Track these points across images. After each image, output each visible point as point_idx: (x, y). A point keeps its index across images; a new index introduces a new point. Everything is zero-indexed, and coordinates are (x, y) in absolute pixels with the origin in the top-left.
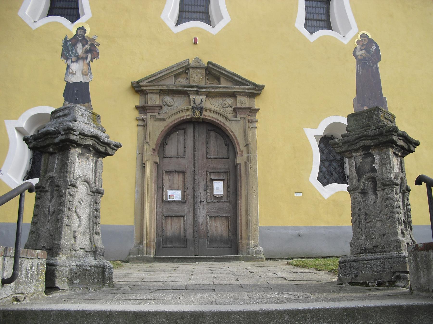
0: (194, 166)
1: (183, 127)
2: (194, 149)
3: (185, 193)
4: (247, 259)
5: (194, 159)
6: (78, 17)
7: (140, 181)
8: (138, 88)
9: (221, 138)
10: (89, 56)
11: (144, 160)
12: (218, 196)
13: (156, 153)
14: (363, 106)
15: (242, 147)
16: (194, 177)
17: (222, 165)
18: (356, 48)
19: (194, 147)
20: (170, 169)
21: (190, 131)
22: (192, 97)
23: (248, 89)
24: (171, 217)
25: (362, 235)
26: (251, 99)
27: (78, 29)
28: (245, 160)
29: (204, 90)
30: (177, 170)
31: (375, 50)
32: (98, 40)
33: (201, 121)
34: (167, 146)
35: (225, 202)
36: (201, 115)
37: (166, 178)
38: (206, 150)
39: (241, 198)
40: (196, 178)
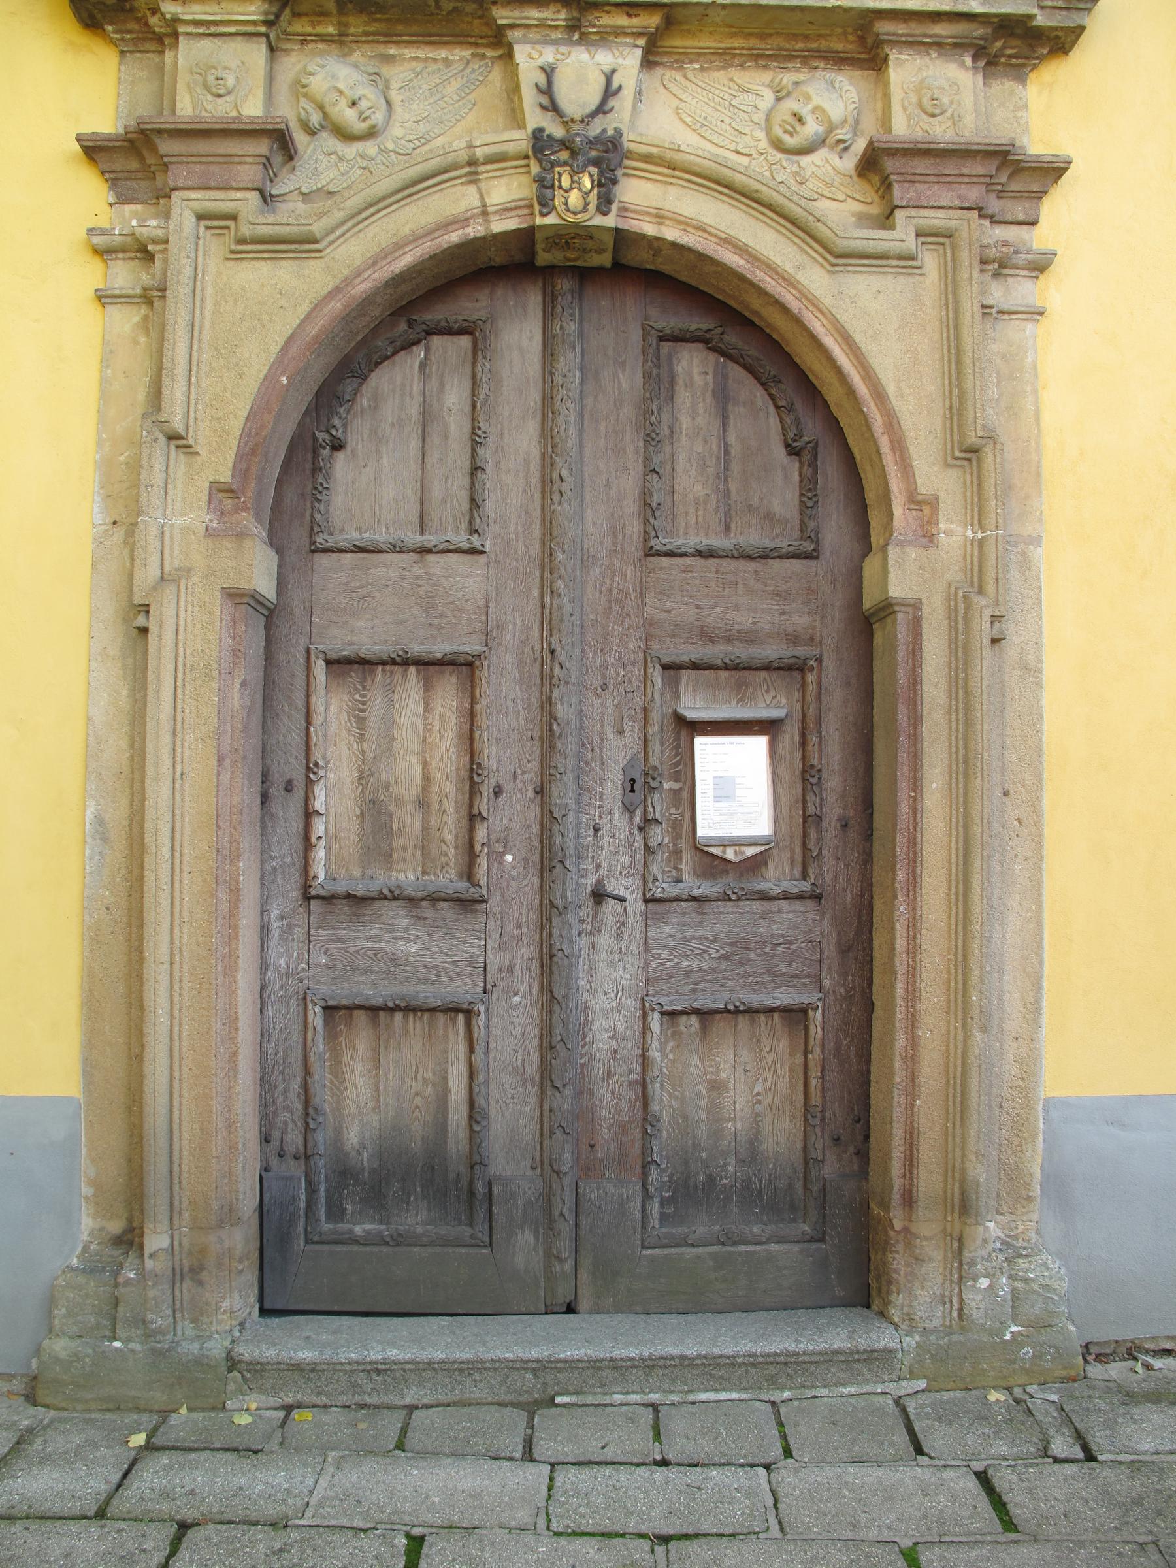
0: (548, 620)
1: (471, 305)
3: (481, 833)
7: (116, 747)
9: (760, 394)
12: (730, 854)
15: (932, 474)
16: (547, 705)
17: (760, 609)
19: (547, 463)
21: (518, 330)
22: (529, 58)
26: (1003, 86)
28: (954, 574)
30: (417, 649)
33: (605, 260)
35: (786, 896)
37: (332, 707)
38: (645, 496)
39: (913, 880)
40: (561, 711)
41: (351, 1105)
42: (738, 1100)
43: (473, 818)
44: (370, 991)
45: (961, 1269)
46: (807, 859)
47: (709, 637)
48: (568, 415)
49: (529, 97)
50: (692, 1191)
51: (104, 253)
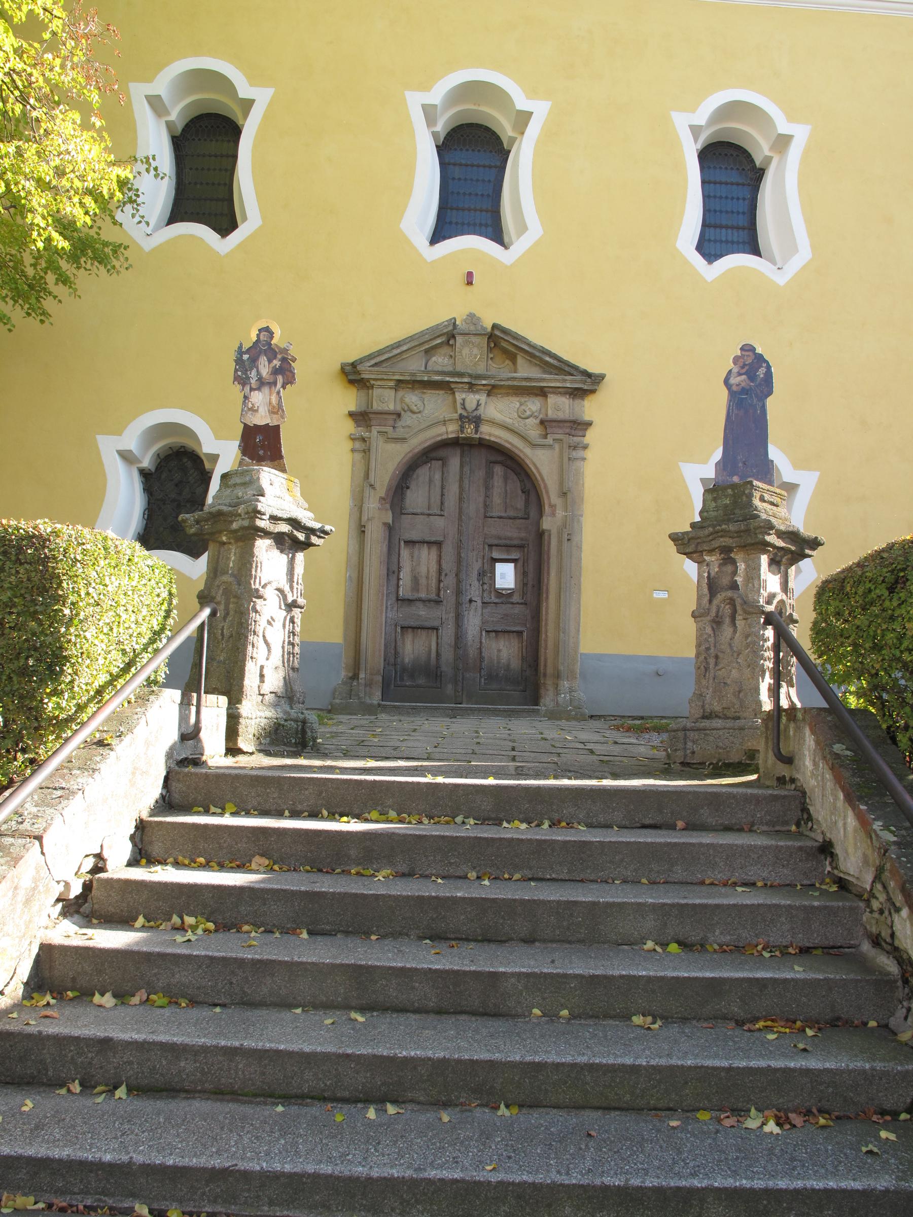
0: (460, 532)
1: (442, 453)
2: (461, 499)
3: (442, 585)
4: (554, 715)
5: (460, 519)
6: (233, 226)
8: (353, 375)
9: (515, 477)
10: (280, 379)
11: (364, 518)
12: (504, 592)
13: (388, 506)
14: (732, 475)
16: (459, 554)
17: (512, 532)
18: (730, 371)
19: (461, 494)
20: (414, 536)
22: (459, 396)
23: (572, 381)
24: (413, 628)
25: (707, 688)
27: (260, 330)
29: (484, 382)
30: (427, 539)
31: (765, 374)
32: (293, 352)
34: (408, 492)
35: (518, 603)
36: (476, 432)
37: (405, 553)
38: (485, 502)
39: (547, 598)
40: (462, 555)
41: (407, 652)
42: (505, 654)
43: (440, 581)
44: (412, 624)
45: (558, 693)
46: (524, 594)
47: (500, 538)
48: (466, 482)
49: (459, 406)
50: (492, 677)
51: (353, 439)
